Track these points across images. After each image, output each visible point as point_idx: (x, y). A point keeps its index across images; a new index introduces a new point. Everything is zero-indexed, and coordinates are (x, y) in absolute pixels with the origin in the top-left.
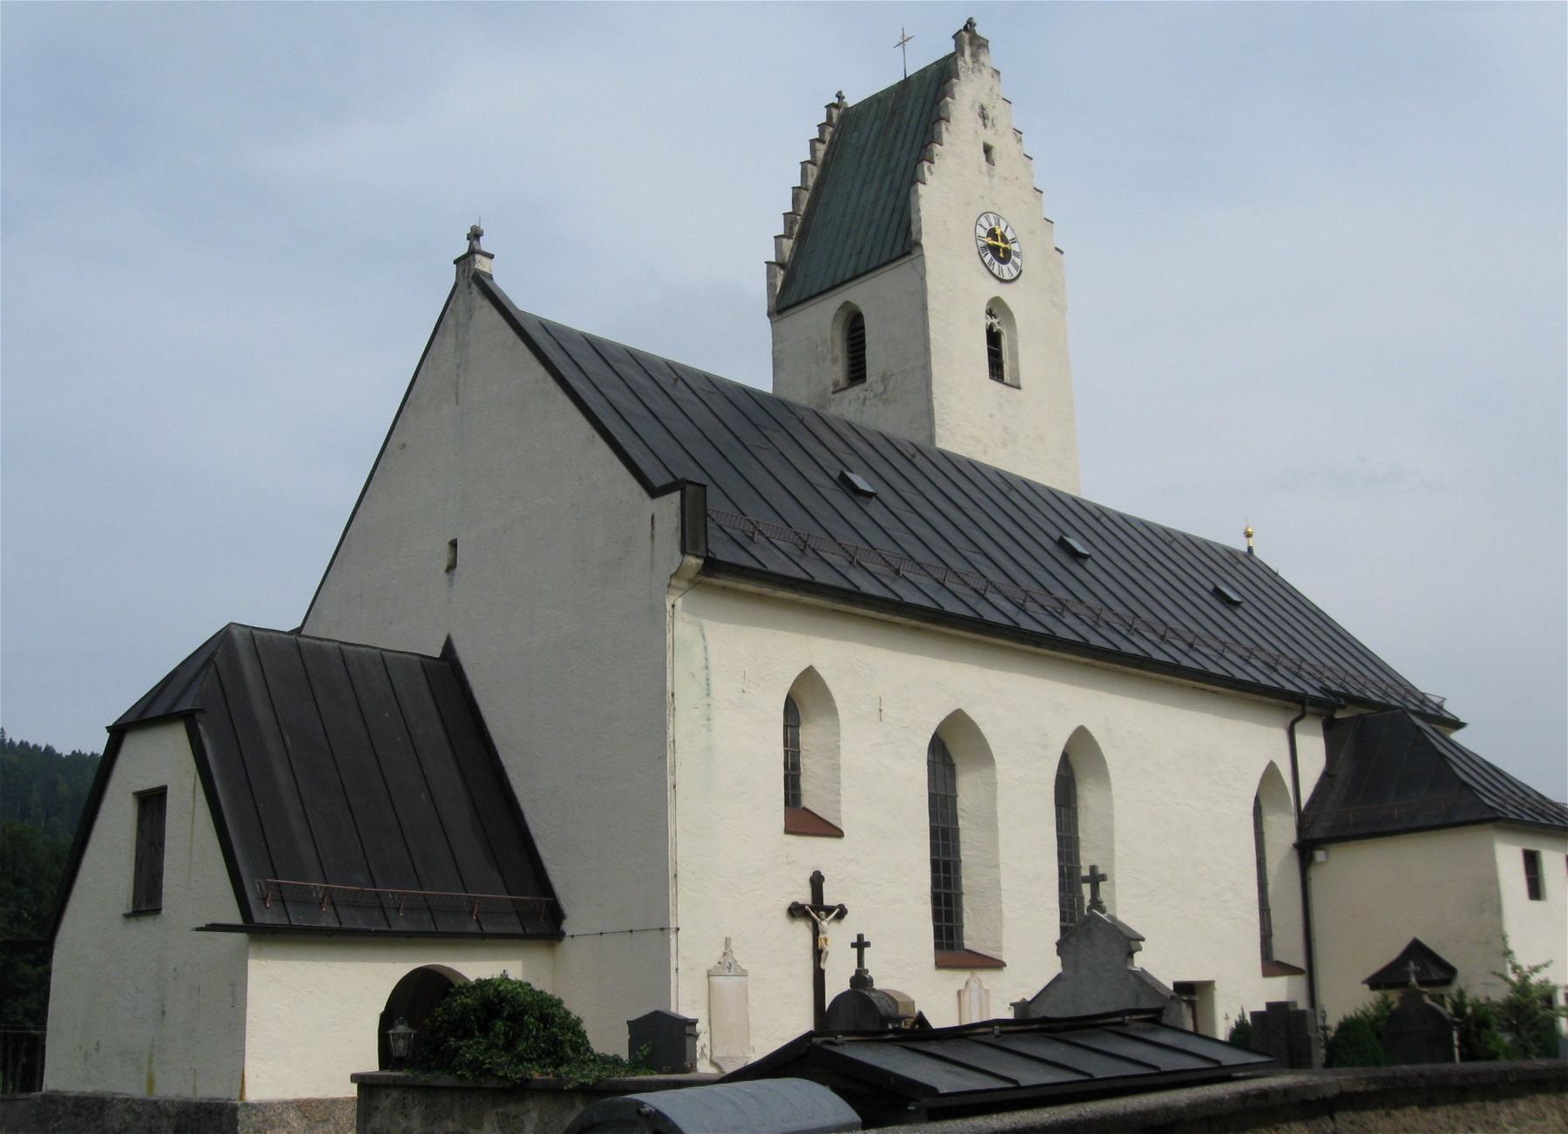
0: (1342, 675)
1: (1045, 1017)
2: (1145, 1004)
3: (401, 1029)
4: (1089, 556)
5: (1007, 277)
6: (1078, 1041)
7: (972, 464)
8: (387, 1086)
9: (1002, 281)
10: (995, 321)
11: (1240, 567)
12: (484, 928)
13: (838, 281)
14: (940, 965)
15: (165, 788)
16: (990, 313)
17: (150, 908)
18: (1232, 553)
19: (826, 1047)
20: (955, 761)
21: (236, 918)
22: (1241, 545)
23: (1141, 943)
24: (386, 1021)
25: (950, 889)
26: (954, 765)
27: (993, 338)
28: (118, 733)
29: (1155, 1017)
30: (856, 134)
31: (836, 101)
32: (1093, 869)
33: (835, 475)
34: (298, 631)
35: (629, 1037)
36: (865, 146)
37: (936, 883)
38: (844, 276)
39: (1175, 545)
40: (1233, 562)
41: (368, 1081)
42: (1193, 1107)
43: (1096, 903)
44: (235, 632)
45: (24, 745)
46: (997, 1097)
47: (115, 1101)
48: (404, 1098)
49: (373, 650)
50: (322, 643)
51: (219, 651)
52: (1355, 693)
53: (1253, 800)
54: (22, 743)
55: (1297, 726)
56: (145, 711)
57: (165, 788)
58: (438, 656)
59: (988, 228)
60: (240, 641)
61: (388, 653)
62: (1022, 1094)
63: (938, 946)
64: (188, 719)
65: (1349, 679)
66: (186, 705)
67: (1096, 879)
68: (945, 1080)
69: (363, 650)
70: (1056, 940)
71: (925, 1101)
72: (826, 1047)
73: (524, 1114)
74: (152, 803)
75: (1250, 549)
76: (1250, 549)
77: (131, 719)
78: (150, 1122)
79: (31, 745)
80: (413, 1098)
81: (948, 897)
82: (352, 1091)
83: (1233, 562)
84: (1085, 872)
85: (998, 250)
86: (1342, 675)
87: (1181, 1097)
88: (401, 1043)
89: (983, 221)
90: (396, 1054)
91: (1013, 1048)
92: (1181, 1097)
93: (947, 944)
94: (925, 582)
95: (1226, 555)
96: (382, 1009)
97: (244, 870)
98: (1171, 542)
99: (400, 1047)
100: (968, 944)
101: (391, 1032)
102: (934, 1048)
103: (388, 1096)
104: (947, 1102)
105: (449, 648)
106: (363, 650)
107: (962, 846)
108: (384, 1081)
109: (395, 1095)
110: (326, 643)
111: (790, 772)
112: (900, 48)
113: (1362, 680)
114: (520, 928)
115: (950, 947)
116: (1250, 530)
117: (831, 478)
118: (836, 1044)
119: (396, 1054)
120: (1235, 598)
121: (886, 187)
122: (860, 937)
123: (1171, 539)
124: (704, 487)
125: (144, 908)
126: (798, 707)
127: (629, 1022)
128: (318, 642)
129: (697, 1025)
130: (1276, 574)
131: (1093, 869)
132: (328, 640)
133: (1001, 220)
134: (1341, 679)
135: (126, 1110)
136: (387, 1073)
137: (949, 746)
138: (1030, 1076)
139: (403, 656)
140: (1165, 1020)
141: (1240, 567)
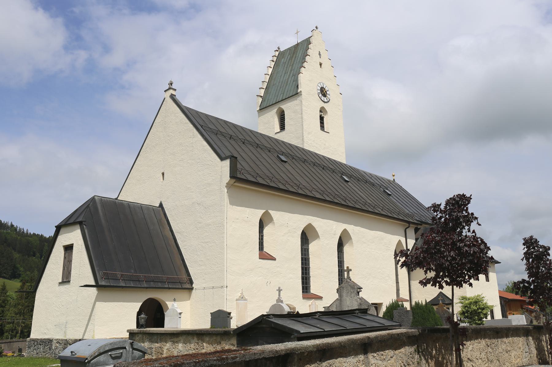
0: (420, 216)
1: (333, 311)
2: (363, 307)
3: (143, 316)
4: (287, 161)
5: (326, 101)
6: (347, 319)
7: (316, 154)
8: (138, 333)
9: (324, 102)
10: (322, 114)
11: (391, 184)
12: (169, 286)
13: (277, 101)
14: (304, 298)
15: (73, 244)
16: (321, 111)
17: (67, 280)
18: (389, 181)
19: (267, 319)
20: (309, 238)
21: (93, 283)
22: (391, 179)
23: (361, 289)
24: (139, 314)
25: (307, 275)
26: (308, 240)
27: (322, 119)
28: (59, 228)
29: (364, 311)
30: (283, 59)
31: (277, 49)
32: (348, 267)
33: (340, 176)
34: (116, 199)
35: (211, 317)
36: (286, 62)
37: (303, 273)
38: (279, 99)
39: (373, 178)
40: (389, 183)
41: (132, 332)
42: (376, 337)
43: (349, 277)
44: (96, 198)
45: (34, 234)
46: (318, 334)
47: (53, 340)
48: (143, 337)
49: (138, 204)
50: (123, 202)
51: (91, 204)
52: (423, 221)
53: (394, 251)
54: (33, 234)
55: (407, 230)
56: (68, 221)
57: (73, 244)
58: (158, 206)
59: (321, 87)
60: (97, 201)
61: (144, 205)
62: (325, 333)
63: (303, 292)
64: (80, 223)
65: (422, 217)
66: (80, 219)
67: (349, 270)
68: (302, 329)
69: (136, 204)
70: (337, 288)
71: (296, 335)
72: (267, 319)
73: (179, 341)
74: (69, 248)
75: (394, 180)
76: (394, 180)
77: (63, 223)
78: (64, 346)
79: (37, 234)
80: (146, 337)
81: (306, 278)
82: (127, 335)
83: (389, 183)
84: (345, 268)
85: (323, 92)
86: (420, 216)
87: (372, 334)
88: (143, 320)
89: (319, 85)
90: (141, 323)
91: (322, 319)
92: (372, 334)
93: (306, 291)
94: (332, 197)
95: (387, 181)
96: (138, 310)
97: (96, 269)
98: (372, 177)
99: (142, 322)
100: (312, 291)
101: (140, 317)
102: (299, 319)
103: (138, 336)
104: (303, 335)
105: (161, 205)
106: (136, 204)
107: (310, 263)
108: (137, 332)
109: (140, 336)
110: (124, 202)
111: (261, 241)
112: (296, 34)
113: (426, 217)
114: (181, 286)
115: (307, 292)
116: (394, 174)
117: (339, 176)
118: (270, 318)
119: (141, 323)
120: (390, 193)
121: (291, 74)
122: (279, 288)
123: (371, 176)
124: (236, 158)
125: (65, 281)
126: (263, 222)
127: (211, 313)
128: (122, 201)
129: (231, 314)
130: (401, 187)
131: (348, 267)
132: (125, 201)
133: (324, 85)
134: (419, 216)
135: (57, 343)
136: (138, 329)
137: (307, 234)
138: (328, 328)
139: (147, 206)
140: (368, 312)
141: (391, 184)
